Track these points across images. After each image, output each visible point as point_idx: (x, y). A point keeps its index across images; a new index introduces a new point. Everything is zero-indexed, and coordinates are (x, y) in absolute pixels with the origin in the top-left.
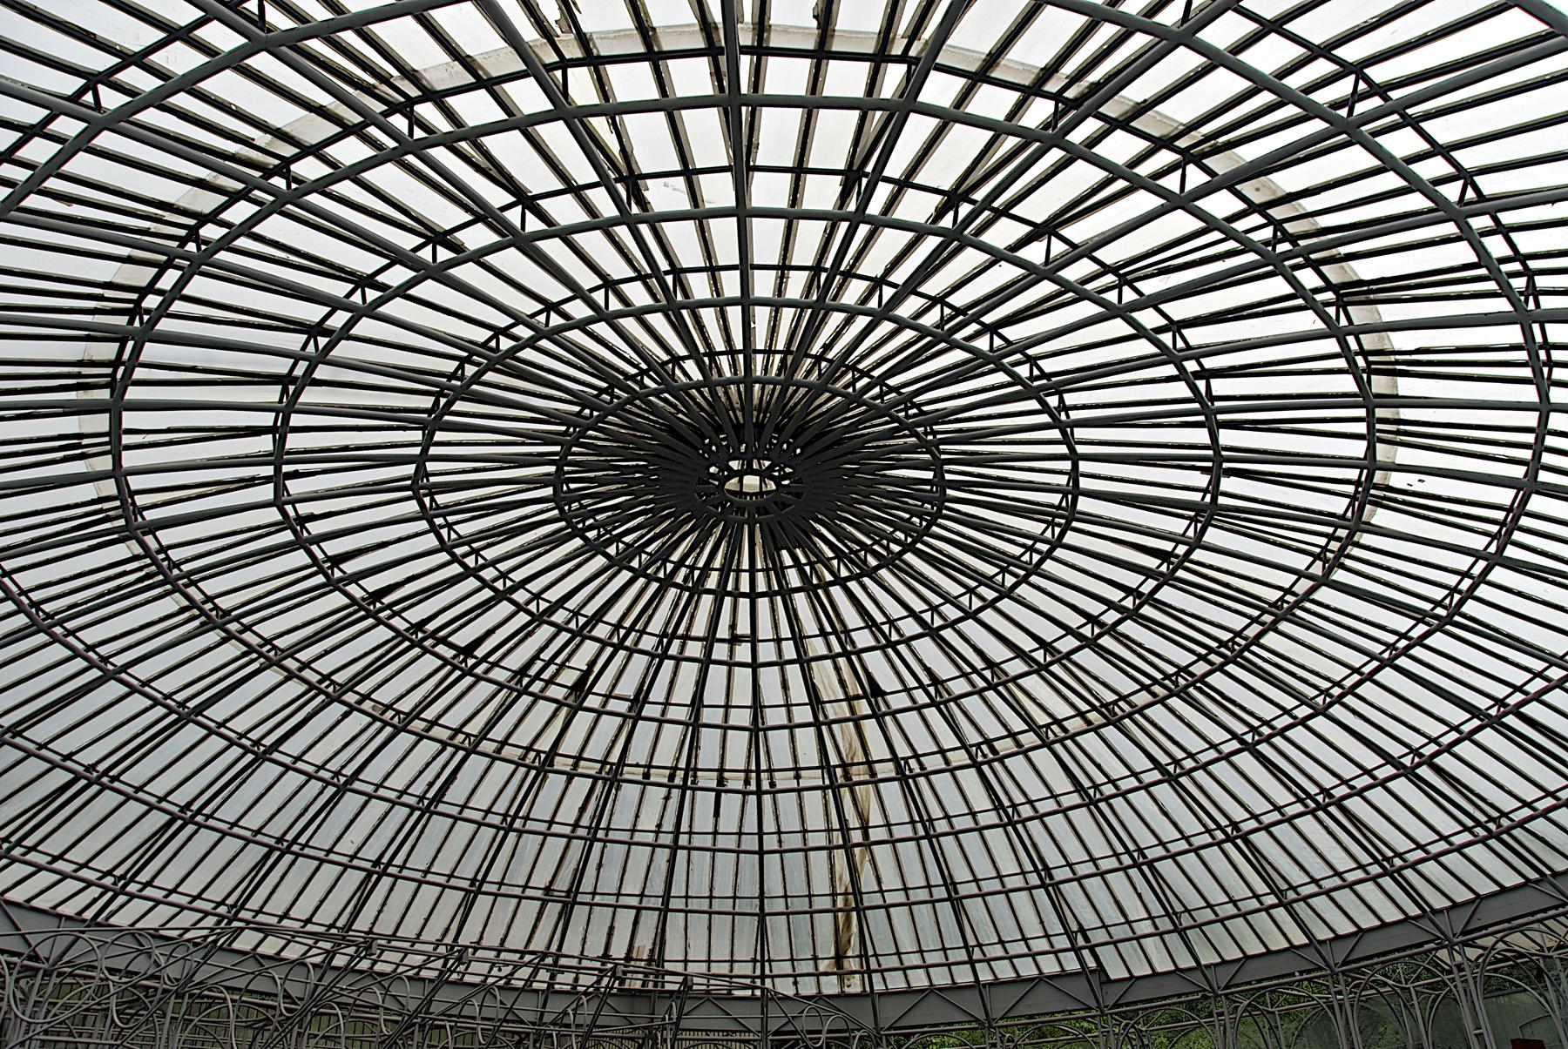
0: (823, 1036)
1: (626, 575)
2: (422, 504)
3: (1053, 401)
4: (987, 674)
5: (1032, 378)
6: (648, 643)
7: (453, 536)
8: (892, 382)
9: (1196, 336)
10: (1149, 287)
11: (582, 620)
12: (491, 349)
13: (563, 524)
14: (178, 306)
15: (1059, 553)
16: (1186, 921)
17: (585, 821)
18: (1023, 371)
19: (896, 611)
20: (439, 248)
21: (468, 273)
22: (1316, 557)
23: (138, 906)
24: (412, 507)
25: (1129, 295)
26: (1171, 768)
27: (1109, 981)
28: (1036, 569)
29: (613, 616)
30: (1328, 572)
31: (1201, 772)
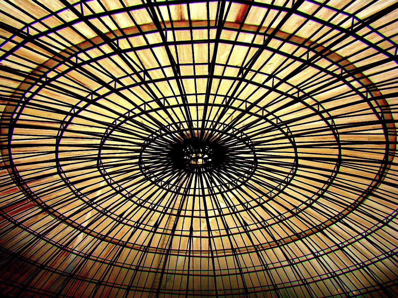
1: (157, 187)
9: (327, 106)
12: (114, 125)
15: (295, 178)
19: (249, 199)
21: (101, 102)
25: (301, 94)
26: (340, 245)
30: (380, 178)
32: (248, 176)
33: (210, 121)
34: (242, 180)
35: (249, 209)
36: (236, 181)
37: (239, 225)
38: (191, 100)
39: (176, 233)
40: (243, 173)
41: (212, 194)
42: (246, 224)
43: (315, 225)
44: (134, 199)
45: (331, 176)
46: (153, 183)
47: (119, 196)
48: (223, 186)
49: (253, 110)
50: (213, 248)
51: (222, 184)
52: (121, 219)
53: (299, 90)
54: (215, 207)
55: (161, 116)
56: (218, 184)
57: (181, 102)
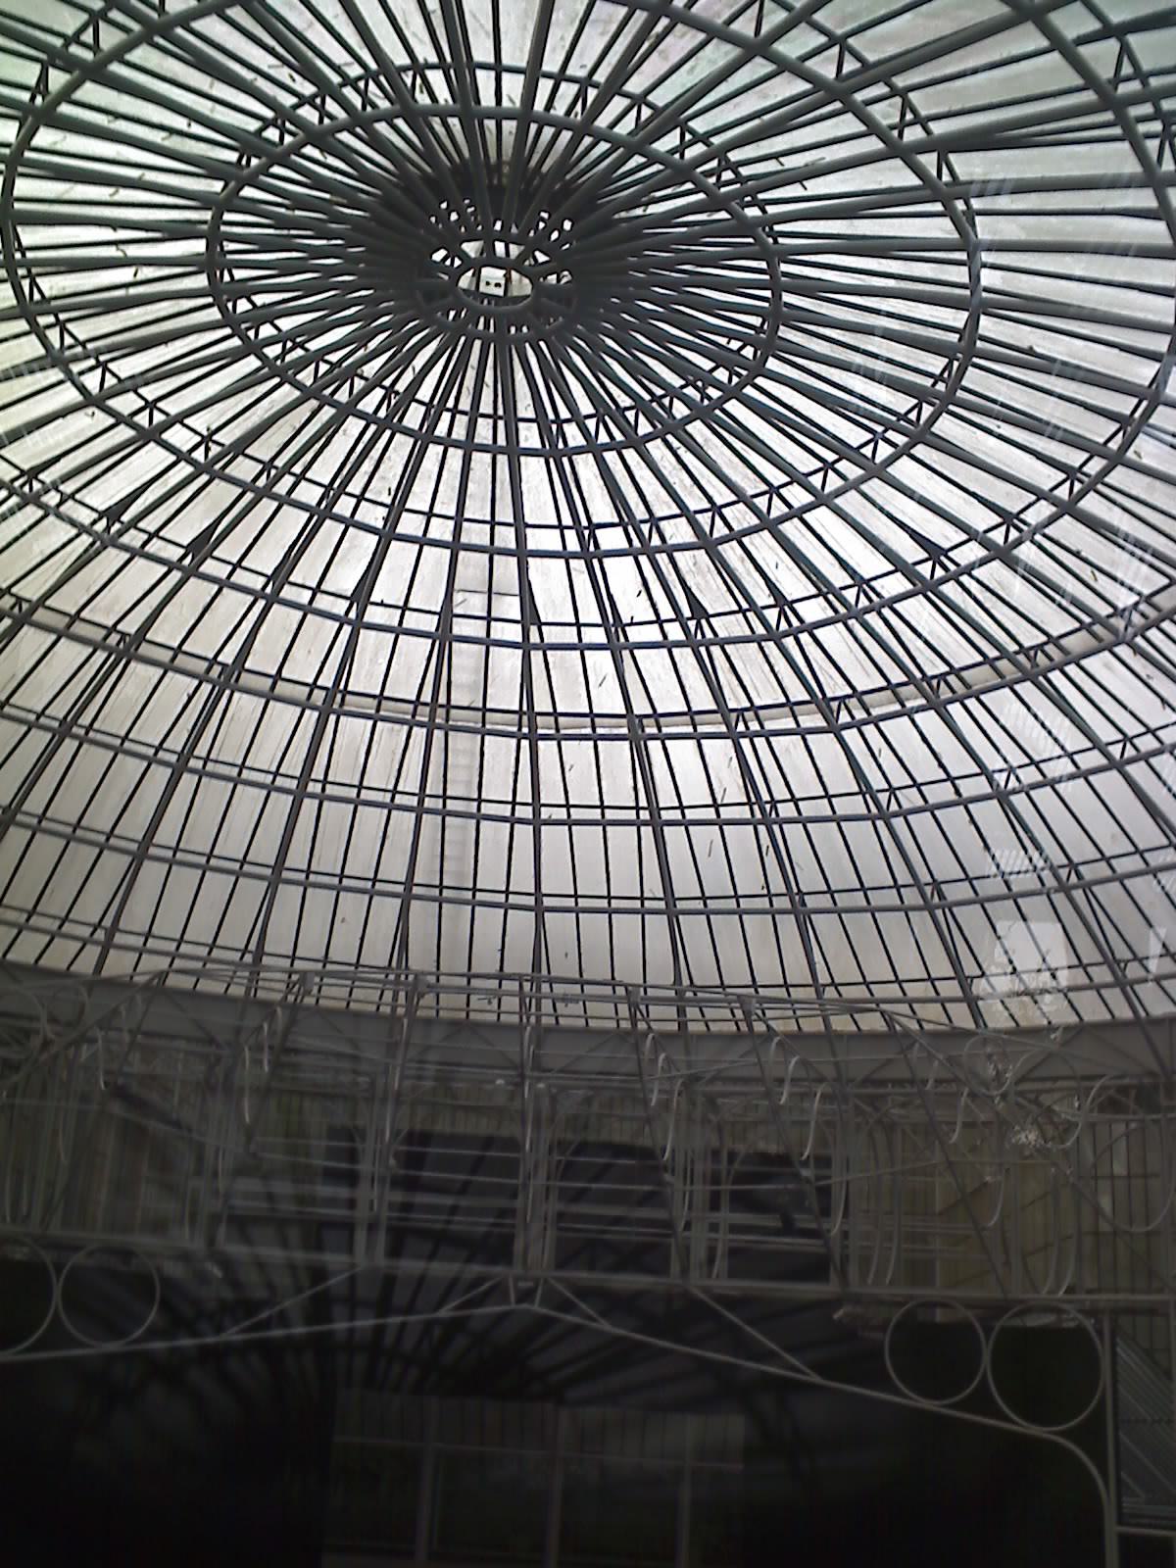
1: (287, 393)
4: (772, 615)
6: (309, 494)
11: (215, 450)
16: (1133, 971)
18: (886, 113)
19: (663, 506)
29: (263, 449)
32: (730, 380)
33: (572, 80)
40: (707, 365)
41: (554, 453)
42: (698, 610)
43: (1013, 647)
44: (178, 436)
46: (307, 394)
47: (153, 458)
49: (792, 47)
50: (542, 704)
51: (604, 410)
54: (567, 520)
56: (585, 407)
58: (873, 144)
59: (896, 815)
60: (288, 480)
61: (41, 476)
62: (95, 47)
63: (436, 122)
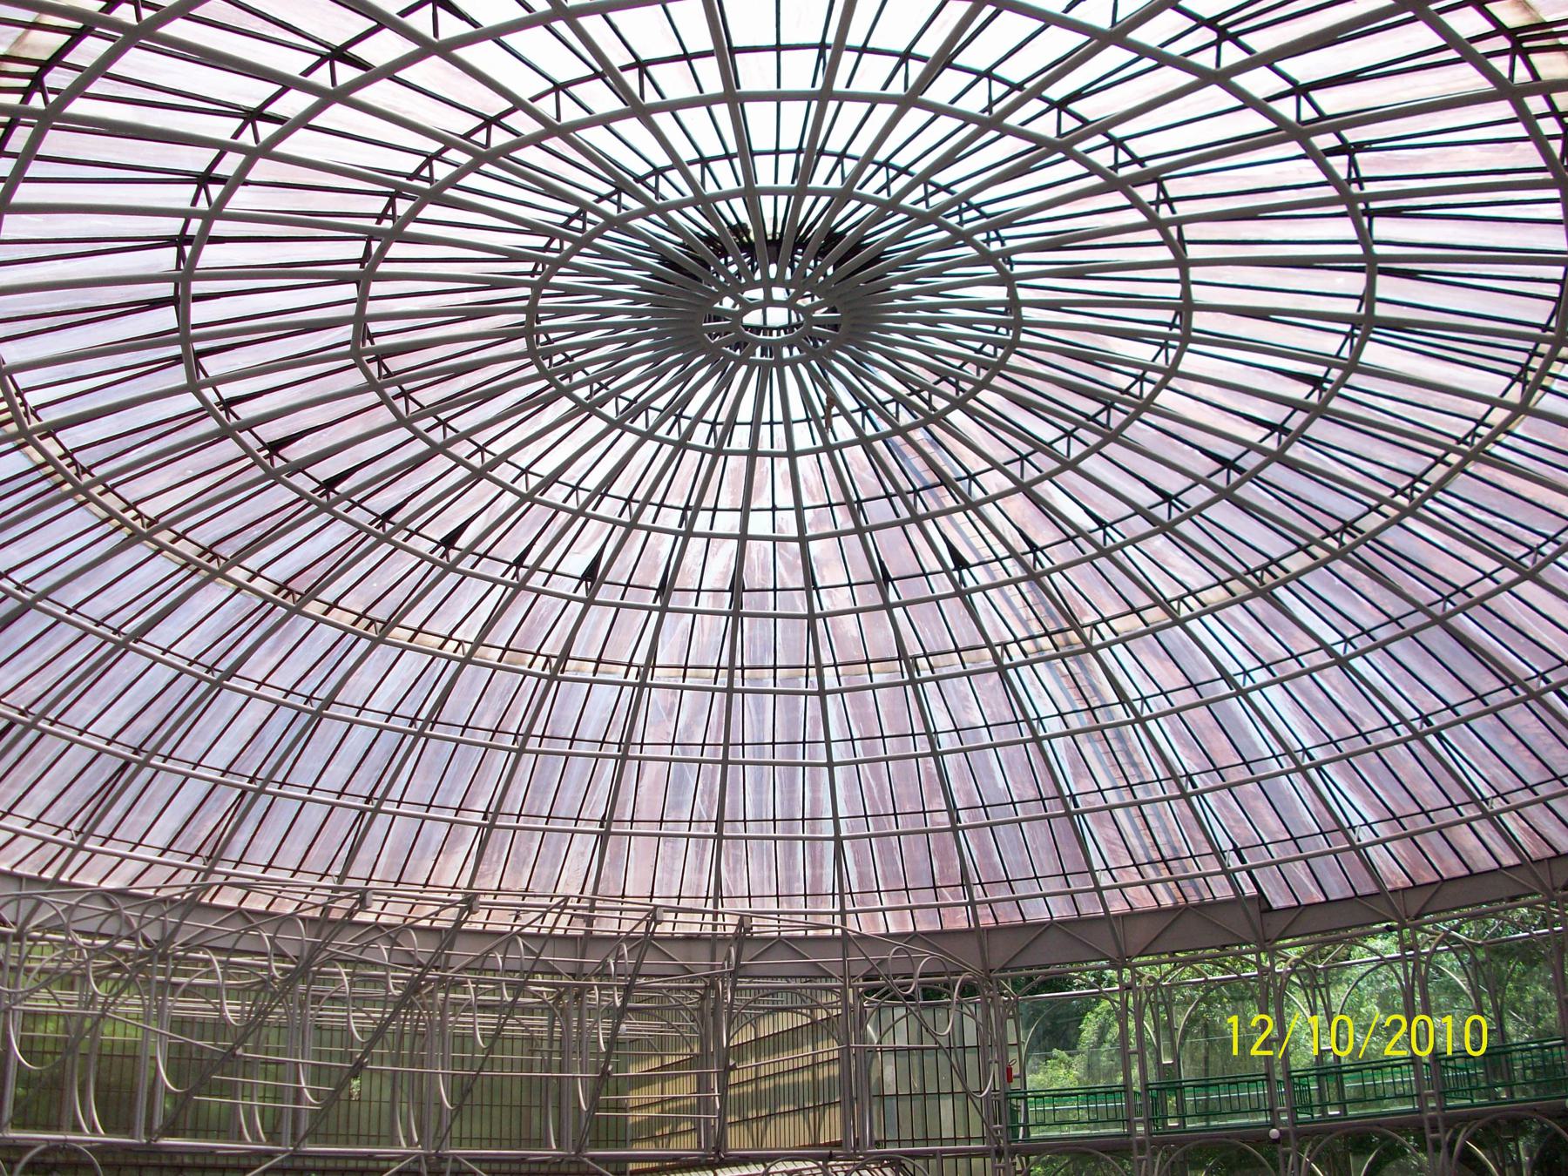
0: (914, 982)
1: (629, 440)
2: (367, 373)
3: (1147, 193)
5: (1117, 166)
7: (413, 407)
8: (942, 178)
9: (1332, 101)
10: (1262, 42)
11: (583, 496)
13: (545, 383)
14: (35, 169)
17: (614, 737)
18: (1104, 158)
19: (974, 463)
20: (338, 64)
22: (1515, 379)
23: (102, 863)
24: (356, 378)
26: (1339, 649)
27: (1270, 909)
28: (1147, 405)
29: (621, 487)
30: (1527, 396)
31: (1359, 659)
34: (951, 391)
35: (975, 506)
36: (925, 394)
37: (932, 564)
38: (755, 73)
39: (676, 600)
42: (960, 563)
43: (1240, 569)
45: (1325, 379)
46: (612, 425)
48: (871, 412)
52: (453, 554)
53: (1223, 35)
55: (631, 146)
57: (713, 85)
58: (1096, 180)
59: (1149, 718)
60: (650, 511)
61: (393, 519)
62: (430, 180)
63: (722, 205)
